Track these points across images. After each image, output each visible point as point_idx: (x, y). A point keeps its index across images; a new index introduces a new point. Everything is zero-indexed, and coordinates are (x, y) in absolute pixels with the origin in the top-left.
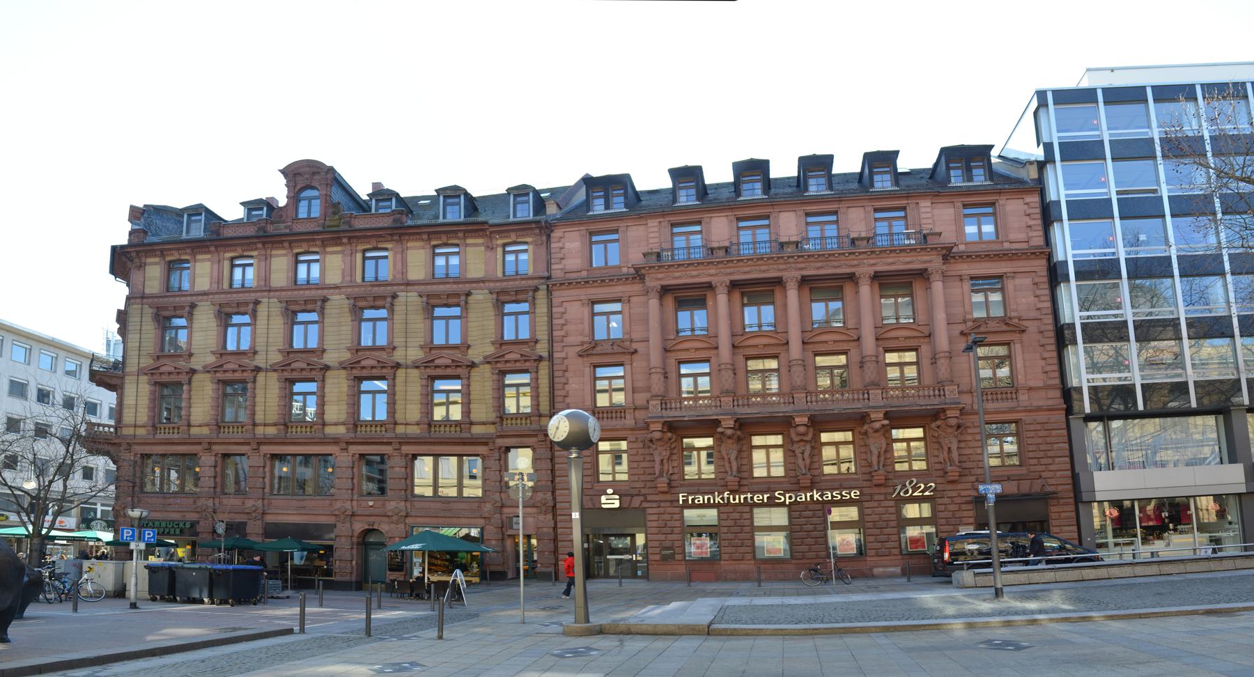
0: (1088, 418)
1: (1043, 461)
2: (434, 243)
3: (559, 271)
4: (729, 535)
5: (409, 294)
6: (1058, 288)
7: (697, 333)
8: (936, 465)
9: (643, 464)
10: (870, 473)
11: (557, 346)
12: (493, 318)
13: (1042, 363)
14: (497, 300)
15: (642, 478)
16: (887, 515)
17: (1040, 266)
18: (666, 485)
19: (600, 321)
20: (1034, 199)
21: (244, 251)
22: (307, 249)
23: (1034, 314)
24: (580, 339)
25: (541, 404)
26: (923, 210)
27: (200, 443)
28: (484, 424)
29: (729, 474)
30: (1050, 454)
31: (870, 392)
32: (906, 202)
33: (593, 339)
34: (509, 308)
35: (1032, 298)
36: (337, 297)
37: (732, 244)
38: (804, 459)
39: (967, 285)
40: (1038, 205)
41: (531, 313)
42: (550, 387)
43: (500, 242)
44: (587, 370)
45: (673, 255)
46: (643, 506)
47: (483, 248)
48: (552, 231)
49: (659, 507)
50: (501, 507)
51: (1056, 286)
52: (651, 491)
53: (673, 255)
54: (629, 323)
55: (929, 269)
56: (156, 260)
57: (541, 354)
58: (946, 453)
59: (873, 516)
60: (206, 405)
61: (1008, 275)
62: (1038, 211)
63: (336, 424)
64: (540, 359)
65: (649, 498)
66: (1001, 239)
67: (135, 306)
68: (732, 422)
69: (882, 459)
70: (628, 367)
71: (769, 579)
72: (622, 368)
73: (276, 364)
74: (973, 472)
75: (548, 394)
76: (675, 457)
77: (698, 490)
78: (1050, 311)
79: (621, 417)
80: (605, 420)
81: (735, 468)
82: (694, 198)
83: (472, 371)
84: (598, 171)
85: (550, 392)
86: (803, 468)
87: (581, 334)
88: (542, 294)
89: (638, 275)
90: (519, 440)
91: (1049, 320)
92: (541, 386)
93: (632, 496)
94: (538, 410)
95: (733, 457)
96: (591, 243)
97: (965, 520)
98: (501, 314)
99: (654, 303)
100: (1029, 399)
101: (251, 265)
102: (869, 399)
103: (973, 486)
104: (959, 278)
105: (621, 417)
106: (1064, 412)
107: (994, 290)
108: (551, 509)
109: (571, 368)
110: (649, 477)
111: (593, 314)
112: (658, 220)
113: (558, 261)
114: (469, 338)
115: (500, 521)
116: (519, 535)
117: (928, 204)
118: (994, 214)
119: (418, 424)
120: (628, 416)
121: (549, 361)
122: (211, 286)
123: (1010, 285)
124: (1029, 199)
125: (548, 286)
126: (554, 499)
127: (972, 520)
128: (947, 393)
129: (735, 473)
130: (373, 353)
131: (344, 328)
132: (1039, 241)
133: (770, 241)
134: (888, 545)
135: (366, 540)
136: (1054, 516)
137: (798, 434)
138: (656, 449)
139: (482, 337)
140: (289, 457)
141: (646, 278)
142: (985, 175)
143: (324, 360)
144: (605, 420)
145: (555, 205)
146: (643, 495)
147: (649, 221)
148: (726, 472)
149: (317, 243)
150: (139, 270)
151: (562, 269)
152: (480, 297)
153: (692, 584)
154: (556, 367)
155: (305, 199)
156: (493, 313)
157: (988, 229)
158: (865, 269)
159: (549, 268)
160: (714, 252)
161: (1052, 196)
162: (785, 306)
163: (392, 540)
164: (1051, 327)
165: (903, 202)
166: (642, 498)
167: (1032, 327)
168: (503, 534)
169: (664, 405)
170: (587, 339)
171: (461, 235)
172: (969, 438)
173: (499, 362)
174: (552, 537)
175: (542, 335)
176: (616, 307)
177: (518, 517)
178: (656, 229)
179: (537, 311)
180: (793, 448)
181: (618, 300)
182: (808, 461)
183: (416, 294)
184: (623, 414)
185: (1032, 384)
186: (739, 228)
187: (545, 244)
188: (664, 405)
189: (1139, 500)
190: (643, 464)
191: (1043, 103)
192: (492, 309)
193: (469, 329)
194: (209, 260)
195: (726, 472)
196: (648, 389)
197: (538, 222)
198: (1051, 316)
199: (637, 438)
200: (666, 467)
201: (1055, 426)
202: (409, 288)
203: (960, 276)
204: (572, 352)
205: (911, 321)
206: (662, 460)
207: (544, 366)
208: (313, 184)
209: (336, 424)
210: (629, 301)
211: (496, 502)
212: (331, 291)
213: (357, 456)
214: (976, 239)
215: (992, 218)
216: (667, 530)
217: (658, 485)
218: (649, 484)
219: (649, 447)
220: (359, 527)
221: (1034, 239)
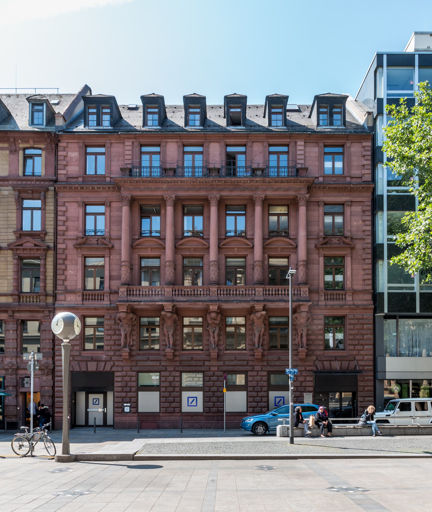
0: (387, 317)
1: (357, 347)
3: (63, 176)
4: (166, 393)
7: (154, 234)
9: (114, 338)
10: (253, 350)
11: (60, 239)
12: (15, 211)
14: (19, 197)
15: (113, 348)
16: (262, 382)
17: (367, 198)
18: (127, 354)
19: (90, 220)
20: (369, 144)
23: (360, 235)
24: (76, 233)
25: (48, 285)
26: (299, 148)
29: (168, 346)
30: (361, 342)
31: (256, 289)
32: (288, 140)
33: (85, 235)
34: (27, 203)
37: (178, 167)
38: (214, 337)
40: (370, 149)
42: (54, 272)
43: (22, 146)
44: (80, 260)
46: (112, 370)
47: (8, 152)
48: (59, 141)
50: (16, 369)
52: (118, 358)
54: (110, 223)
57: (48, 244)
59: (254, 382)
62: (369, 153)
64: (48, 248)
66: (345, 175)
68: (171, 308)
69: (261, 340)
70: (107, 259)
71: (188, 428)
72: (103, 259)
74: (315, 353)
75: (52, 278)
76: (134, 333)
78: (370, 233)
79: (101, 299)
80: (90, 300)
81: (171, 342)
82: (156, 123)
84: (92, 89)
85: (54, 276)
86: (213, 344)
87: (77, 230)
88: (51, 194)
90: (31, 314)
91: (369, 240)
92: (48, 270)
94: (46, 292)
95: (171, 333)
96: (86, 154)
97: (308, 389)
98: (21, 209)
99: (125, 210)
100: (353, 300)
101: (40, 155)
102: (255, 294)
103: (314, 363)
105: (101, 299)
106: (372, 311)
107: (338, 214)
108: (51, 371)
109: (69, 257)
110: (117, 348)
111: (86, 214)
112: (132, 140)
113: (62, 167)
115: (15, 380)
116: (30, 393)
117: (303, 143)
121: (54, 250)
123: (348, 211)
125: (55, 188)
127: (312, 389)
128: (302, 293)
129: (171, 346)
133: (203, 167)
134: (261, 404)
136: (360, 389)
137: (211, 319)
138: (123, 326)
139: (6, 226)
141: (122, 189)
144: (90, 300)
145: (62, 118)
151: (65, 174)
152: (6, 193)
153: (141, 431)
154: (59, 256)
156: (15, 207)
157: (339, 165)
159: (56, 174)
160: (167, 172)
162: (209, 218)
164: (370, 246)
165: (287, 141)
167: (359, 245)
168: (17, 392)
169: (129, 292)
170: (80, 235)
173: (19, 249)
174: (51, 394)
175: (50, 229)
176: (101, 209)
177: (29, 377)
178: (130, 148)
179: (47, 208)
180: (208, 329)
182: (216, 339)
185: (356, 287)
186: (184, 153)
187: (54, 151)
188: (129, 292)
189: (412, 380)
190: (114, 338)
191: (380, 65)
192: (15, 203)
195: (166, 345)
196: (119, 278)
197: (49, 133)
198: (370, 237)
199: (111, 316)
200: (128, 340)
201: (366, 321)
204: (70, 244)
207: (51, 253)
210: (110, 205)
211: (13, 365)
214: (330, 173)
215: (341, 157)
216: (127, 389)
217: (123, 354)
218: (117, 353)
219: (118, 324)
221: (366, 175)
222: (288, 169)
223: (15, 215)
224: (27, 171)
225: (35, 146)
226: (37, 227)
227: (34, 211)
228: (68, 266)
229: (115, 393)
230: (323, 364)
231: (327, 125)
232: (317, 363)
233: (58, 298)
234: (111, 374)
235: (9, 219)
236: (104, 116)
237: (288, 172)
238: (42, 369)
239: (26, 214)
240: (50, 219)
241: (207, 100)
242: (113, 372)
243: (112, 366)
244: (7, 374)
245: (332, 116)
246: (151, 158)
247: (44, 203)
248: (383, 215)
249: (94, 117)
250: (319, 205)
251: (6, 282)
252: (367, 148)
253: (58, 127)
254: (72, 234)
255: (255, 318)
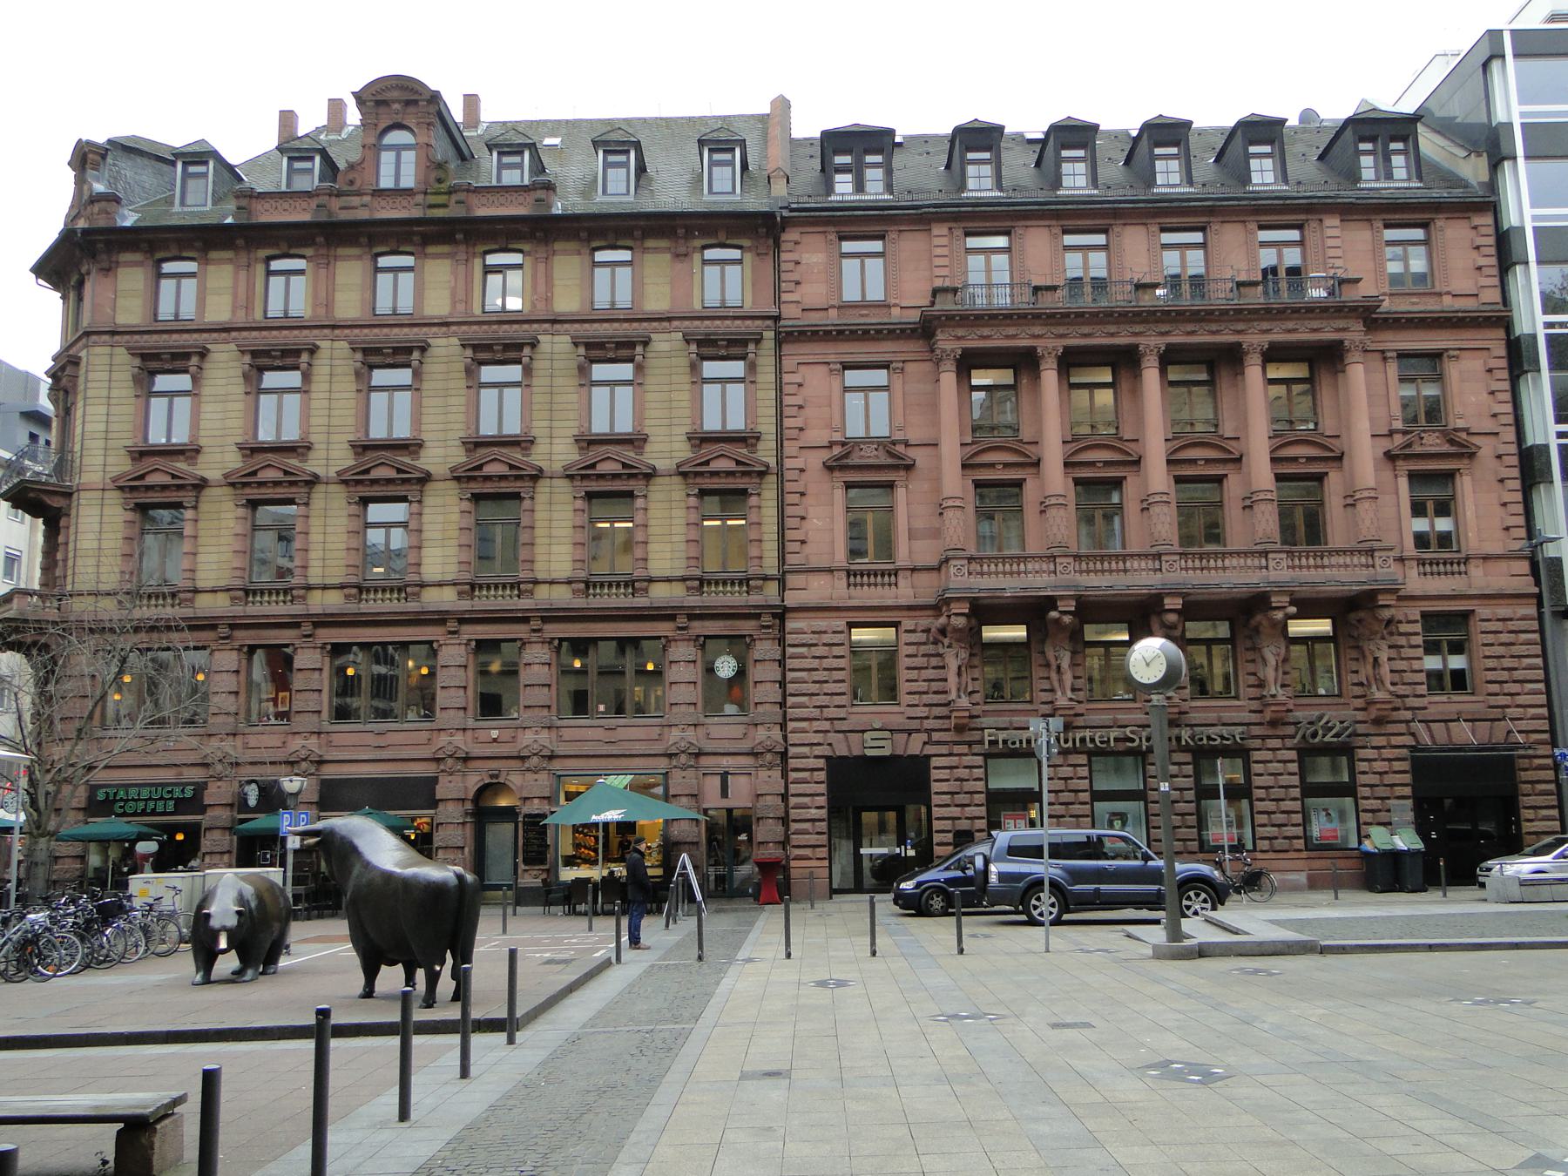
2: (595, 244)
5: (557, 338)
6: (1522, 380)
8: (1356, 688)
11: (790, 448)
13: (1500, 511)
17: (1495, 343)
21: (290, 247)
22: (395, 248)
23: (1489, 425)
27: (213, 627)
28: (668, 580)
35: (1485, 395)
36: (443, 342)
39: (1393, 369)
41: (749, 380)
45: (989, 296)
46: (925, 753)
49: (950, 755)
51: (1518, 377)
53: (989, 296)
55: (1346, 343)
56: (138, 257)
58: (1369, 667)
60: (223, 549)
61: (1452, 353)
62: (1491, 241)
63: (440, 585)
65: (936, 736)
67: (98, 350)
73: (345, 471)
77: (1011, 723)
78: (1510, 419)
83: (651, 482)
89: (925, 330)
91: (1509, 434)
93: (909, 732)
100: (1485, 575)
101: (301, 272)
104: (1378, 356)
114: (647, 422)
118: (1426, 242)
119: (569, 582)
120: (901, 582)
122: (234, 312)
124: (1478, 220)
126: (785, 738)
127: (1407, 791)
130: (504, 450)
131: (453, 401)
132: (1493, 296)
135: (482, 804)
139: (666, 422)
140: (355, 648)
142: (1407, 167)
143: (422, 460)
146: (927, 731)
147: (933, 225)
148: (1052, 690)
149: (415, 238)
150: (106, 276)
155: (390, 147)
158: (1255, 338)
161: (1511, 218)
163: (528, 802)
166: (924, 737)
167: (1486, 448)
171: (637, 233)
172: (1402, 641)
173: (701, 474)
175: (767, 427)
176: (880, 377)
179: (760, 378)
181: (885, 366)
183: (568, 338)
184: (893, 578)
193: (647, 405)
194: (230, 261)
202: (557, 326)
203: (1383, 352)
204: (815, 460)
205: (1311, 426)
206: (959, 667)
208: (405, 123)
209: (440, 585)
212: (435, 329)
213: (474, 643)
220: (473, 782)
222: (1012, 289)
223: (686, 396)
224: (270, 308)
225: (728, 242)
226: (736, 423)
227: (176, 400)
228: (811, 510)
229: (1360, 801)
230: (1448, 729)
231: (991, 190)
232: (1420, 728)
233: (789, 584)
234: (920, 765)
235: (674, 404)
236: (1362, 158)
237: (1012, 296)
238: (757, 754)
239: (488, 396)
240: (768, 403)
241: (69, 158)
242: (929, 757)
243: (925, 743)
244: (675, 767)
245: (1060, 167)
246: (988, 262)
247: (752, 368)
248: (1537, 383)
249: (878, 173)
250: (1385, 359)
251: (668, 547)
252: (1483, 230)
253: (776, 199)
254: (818, 435)
255: (1265, 623)
